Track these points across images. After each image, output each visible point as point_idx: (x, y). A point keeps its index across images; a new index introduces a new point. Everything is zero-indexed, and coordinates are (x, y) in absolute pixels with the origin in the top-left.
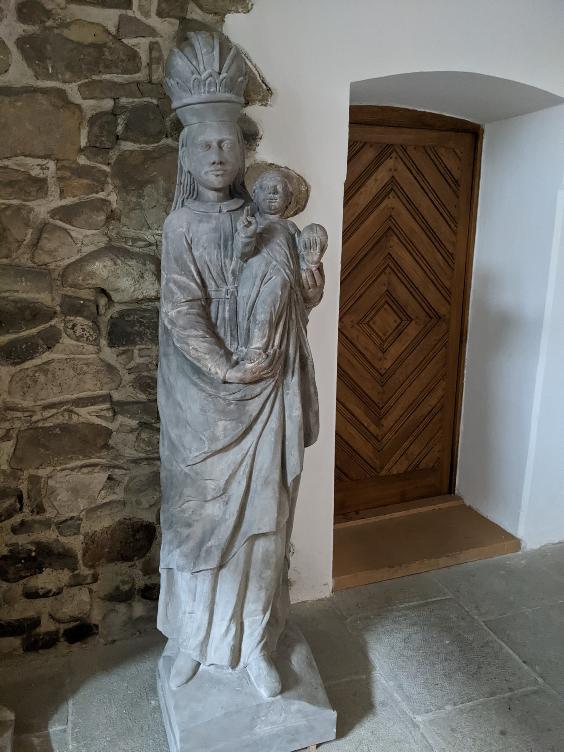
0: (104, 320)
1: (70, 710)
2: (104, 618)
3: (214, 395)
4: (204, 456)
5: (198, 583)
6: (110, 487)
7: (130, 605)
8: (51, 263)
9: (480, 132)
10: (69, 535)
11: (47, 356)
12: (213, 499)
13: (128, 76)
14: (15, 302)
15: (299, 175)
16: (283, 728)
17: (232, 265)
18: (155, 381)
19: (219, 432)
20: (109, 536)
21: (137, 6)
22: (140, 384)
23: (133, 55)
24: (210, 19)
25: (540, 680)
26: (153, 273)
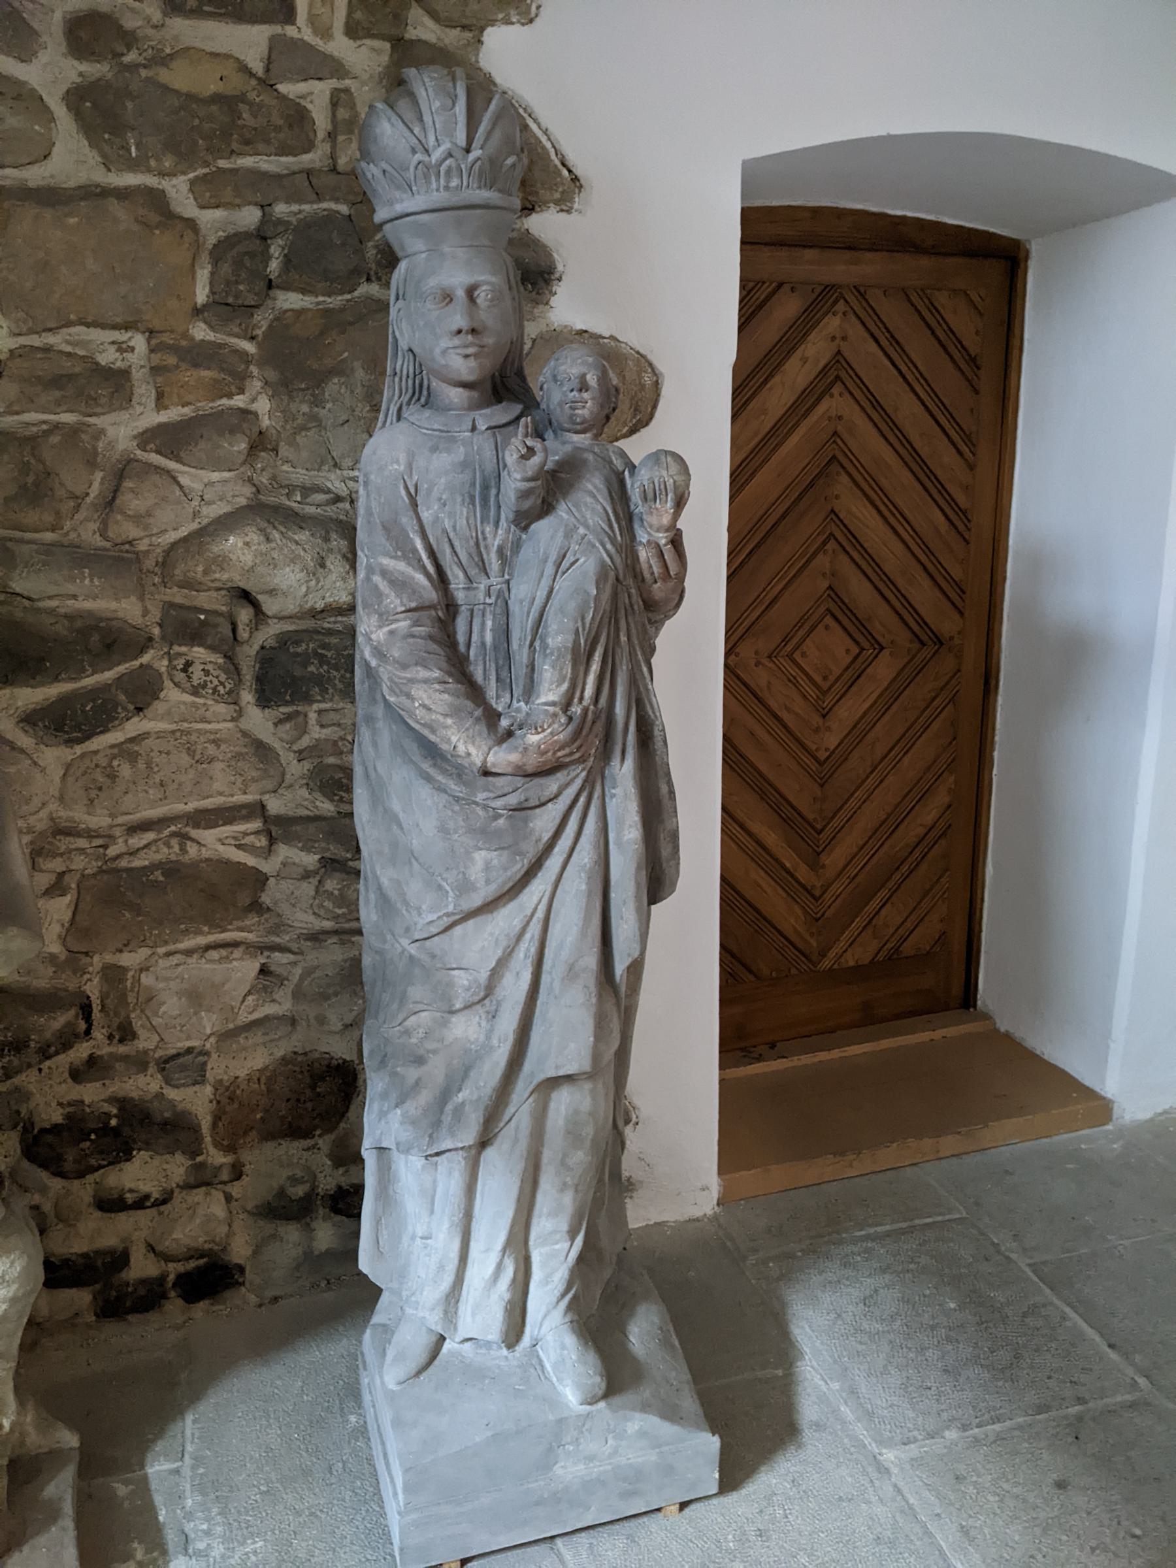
0: (248, 654)
1: (188, 1433)
2: (256, 1252)
3: (463, 799)
4: (447, 921)
5: (439, 1177)
6: (265, 988)
7: (308, 1229)
8: (141, 539)
9: (1022, 254)
10: (183, 1085)
11: (134, 726)
12: (466, 1007)
13: (290, 159)
14: (69, 617)
15: (638, 353)
16: (610, 1467)
17: (497, 537)
18: (348, 772)
19: (476, 872)
20: (263, 1087)
21: (305, 16)
22: (321, 781)
23: (298, 116)
24: (452, 37)
25: (1142, 1381)
26: (344, 556)
